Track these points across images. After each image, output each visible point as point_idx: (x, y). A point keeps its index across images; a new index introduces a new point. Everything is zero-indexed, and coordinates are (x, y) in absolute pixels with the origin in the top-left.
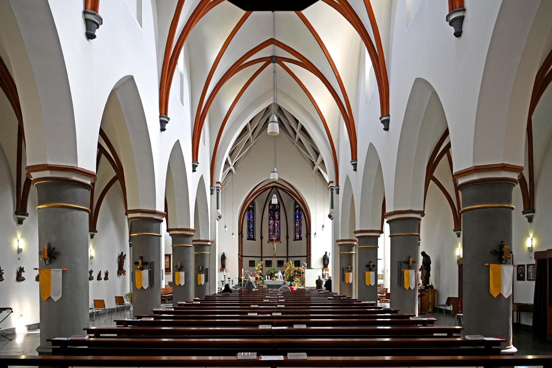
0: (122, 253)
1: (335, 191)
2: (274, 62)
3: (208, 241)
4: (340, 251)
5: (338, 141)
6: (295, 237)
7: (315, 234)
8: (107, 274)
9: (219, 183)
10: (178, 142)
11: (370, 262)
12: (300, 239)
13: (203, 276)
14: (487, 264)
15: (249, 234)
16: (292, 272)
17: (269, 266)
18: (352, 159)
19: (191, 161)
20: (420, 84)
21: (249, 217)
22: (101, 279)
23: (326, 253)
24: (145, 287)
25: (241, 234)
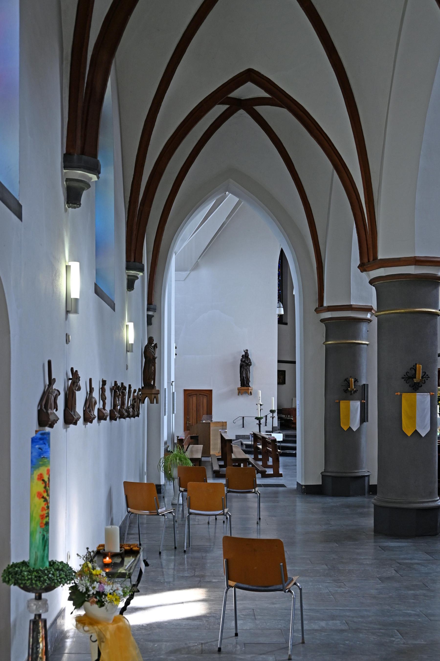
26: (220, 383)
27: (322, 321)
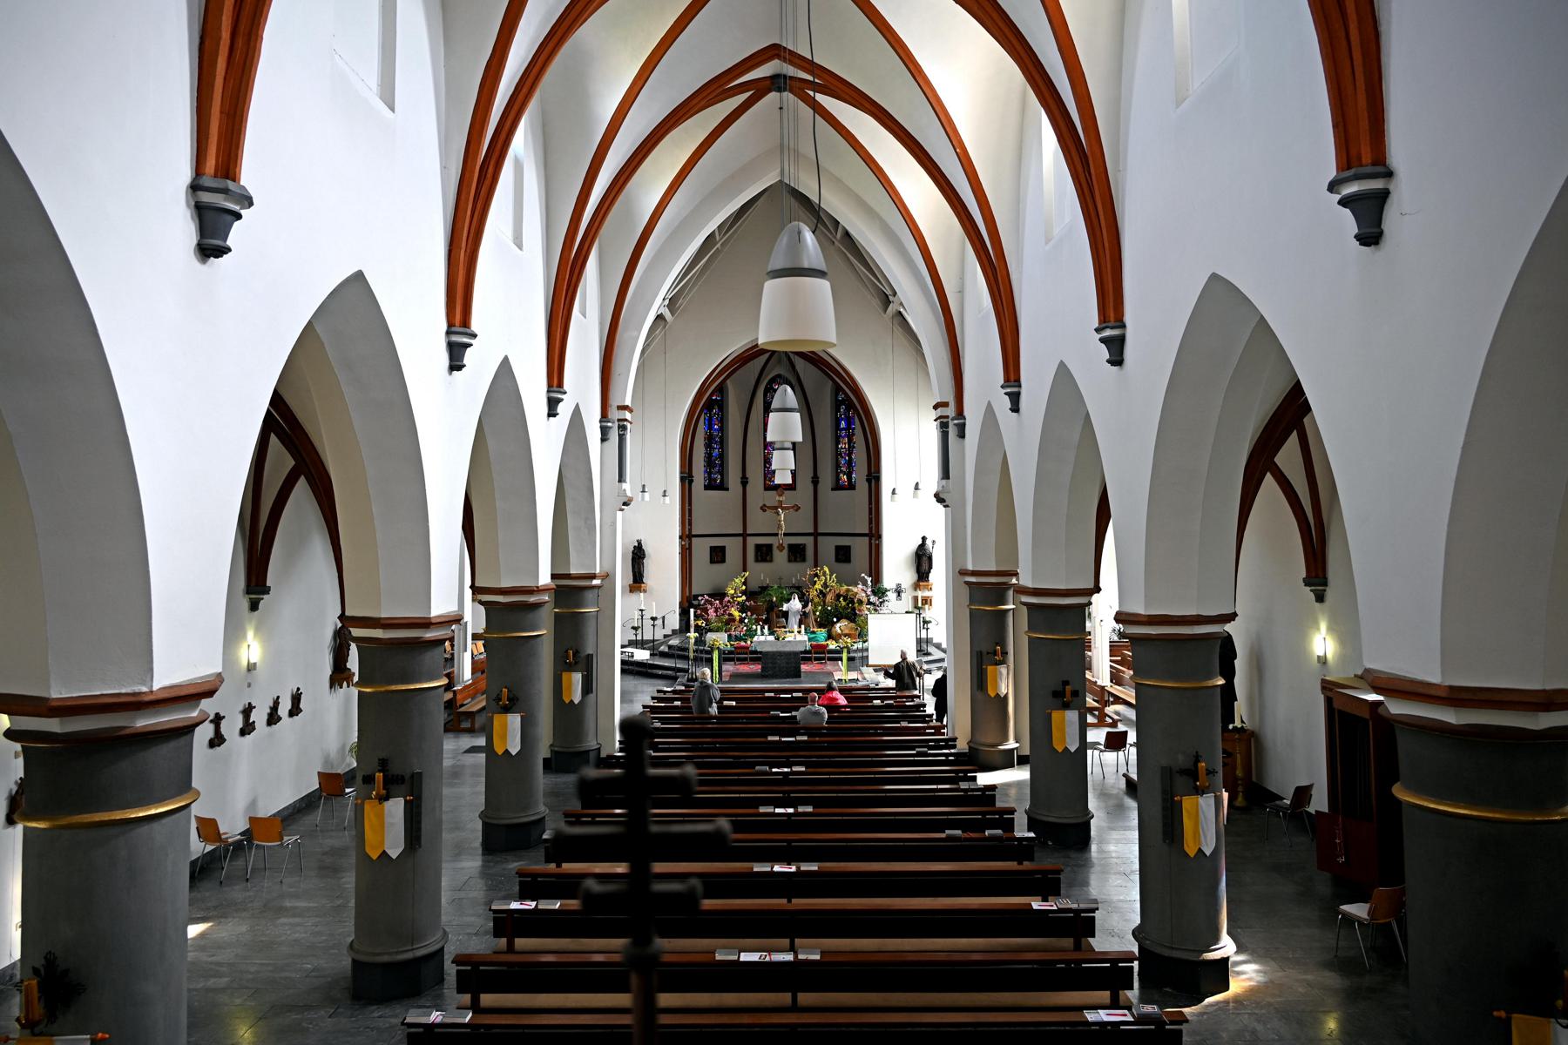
1: (952, 431)
2: (779, 90)
3: (593, 577)
4: (972, 601)
5: (961, 291)
6: (838, 479)
7: (894, 492)
8: (296, 698)
9: (625, 408)
10: (506, 359)
11: (1066, 683)
12: (851, 486)
13: (577, 678)
14: (1503, 1014)
15: (710, 474)
16: (829, 598)
17: (764, 560)
18: (1007, 380)
19: (545, 388)
20: (1220, 295)
21: (710, 427)
22: (279, 719)
23: (924, 539)
25: (686, 479)
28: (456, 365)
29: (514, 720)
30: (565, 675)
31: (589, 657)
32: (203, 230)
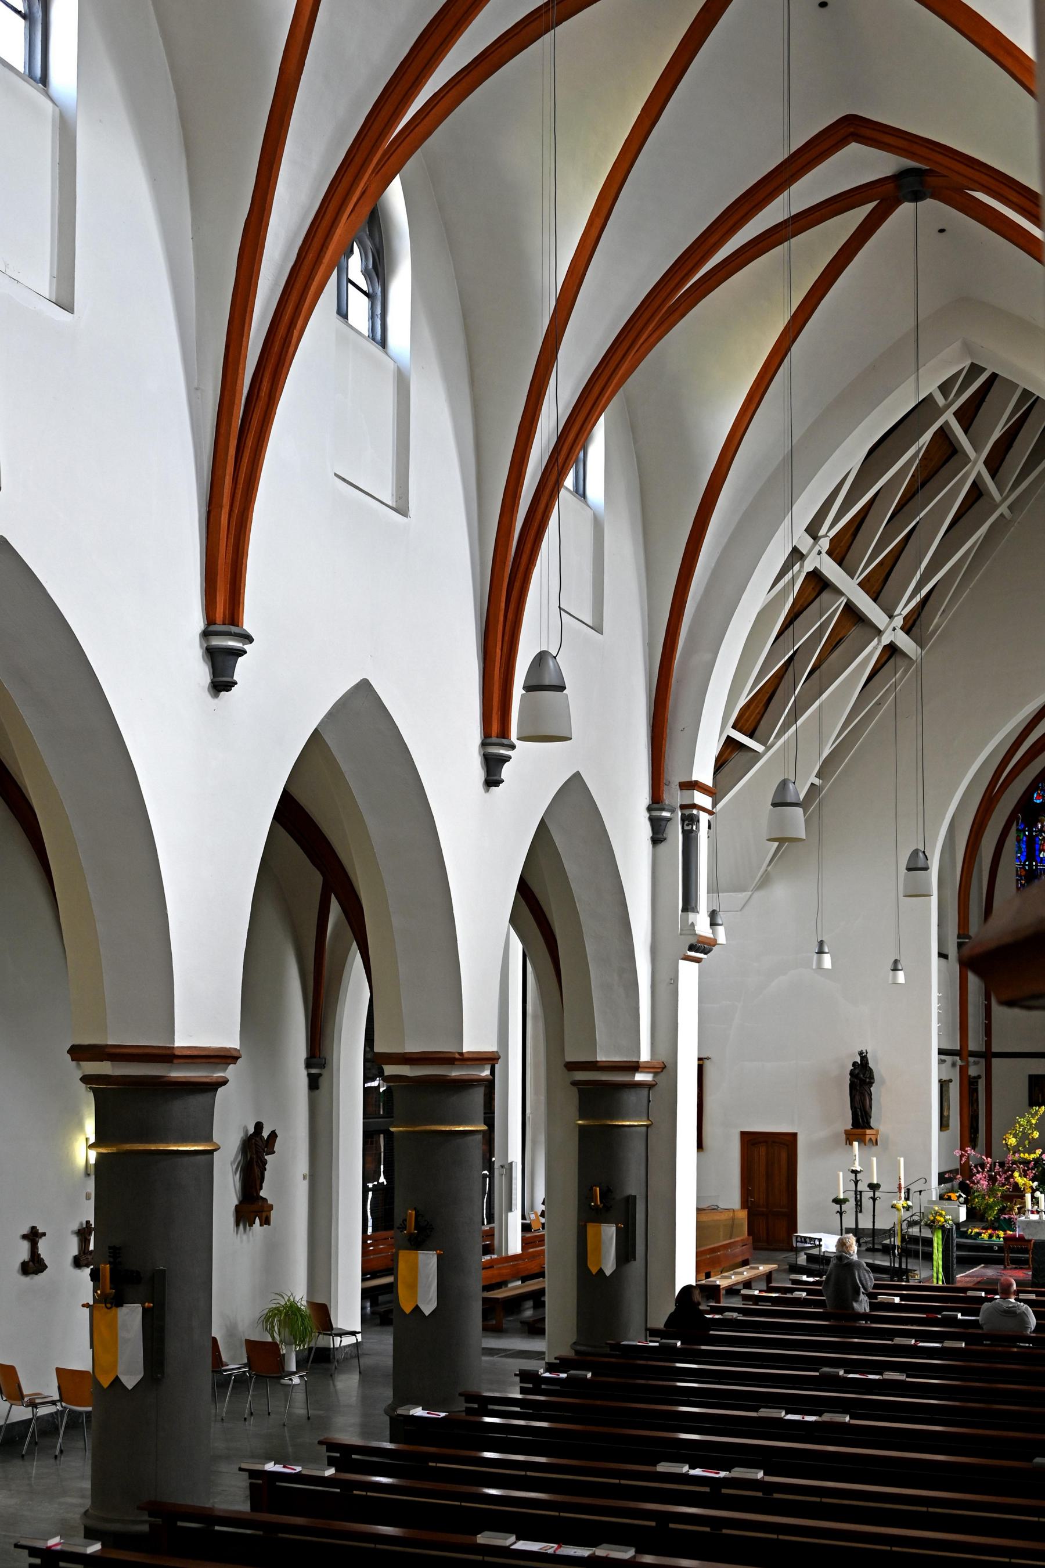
0: (259, 1126)
13: (610, 1232)
24: (130, 1382)
26: (813, 1121)
27: (574, 1083)
28: (492, 781)
29: (428, 1261)
30: (591, 1228)
31: (630, 1202)
32: (215, 671)
